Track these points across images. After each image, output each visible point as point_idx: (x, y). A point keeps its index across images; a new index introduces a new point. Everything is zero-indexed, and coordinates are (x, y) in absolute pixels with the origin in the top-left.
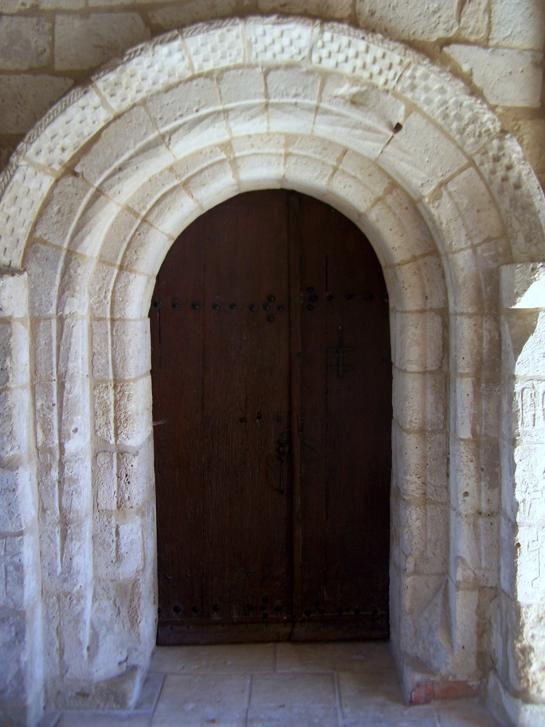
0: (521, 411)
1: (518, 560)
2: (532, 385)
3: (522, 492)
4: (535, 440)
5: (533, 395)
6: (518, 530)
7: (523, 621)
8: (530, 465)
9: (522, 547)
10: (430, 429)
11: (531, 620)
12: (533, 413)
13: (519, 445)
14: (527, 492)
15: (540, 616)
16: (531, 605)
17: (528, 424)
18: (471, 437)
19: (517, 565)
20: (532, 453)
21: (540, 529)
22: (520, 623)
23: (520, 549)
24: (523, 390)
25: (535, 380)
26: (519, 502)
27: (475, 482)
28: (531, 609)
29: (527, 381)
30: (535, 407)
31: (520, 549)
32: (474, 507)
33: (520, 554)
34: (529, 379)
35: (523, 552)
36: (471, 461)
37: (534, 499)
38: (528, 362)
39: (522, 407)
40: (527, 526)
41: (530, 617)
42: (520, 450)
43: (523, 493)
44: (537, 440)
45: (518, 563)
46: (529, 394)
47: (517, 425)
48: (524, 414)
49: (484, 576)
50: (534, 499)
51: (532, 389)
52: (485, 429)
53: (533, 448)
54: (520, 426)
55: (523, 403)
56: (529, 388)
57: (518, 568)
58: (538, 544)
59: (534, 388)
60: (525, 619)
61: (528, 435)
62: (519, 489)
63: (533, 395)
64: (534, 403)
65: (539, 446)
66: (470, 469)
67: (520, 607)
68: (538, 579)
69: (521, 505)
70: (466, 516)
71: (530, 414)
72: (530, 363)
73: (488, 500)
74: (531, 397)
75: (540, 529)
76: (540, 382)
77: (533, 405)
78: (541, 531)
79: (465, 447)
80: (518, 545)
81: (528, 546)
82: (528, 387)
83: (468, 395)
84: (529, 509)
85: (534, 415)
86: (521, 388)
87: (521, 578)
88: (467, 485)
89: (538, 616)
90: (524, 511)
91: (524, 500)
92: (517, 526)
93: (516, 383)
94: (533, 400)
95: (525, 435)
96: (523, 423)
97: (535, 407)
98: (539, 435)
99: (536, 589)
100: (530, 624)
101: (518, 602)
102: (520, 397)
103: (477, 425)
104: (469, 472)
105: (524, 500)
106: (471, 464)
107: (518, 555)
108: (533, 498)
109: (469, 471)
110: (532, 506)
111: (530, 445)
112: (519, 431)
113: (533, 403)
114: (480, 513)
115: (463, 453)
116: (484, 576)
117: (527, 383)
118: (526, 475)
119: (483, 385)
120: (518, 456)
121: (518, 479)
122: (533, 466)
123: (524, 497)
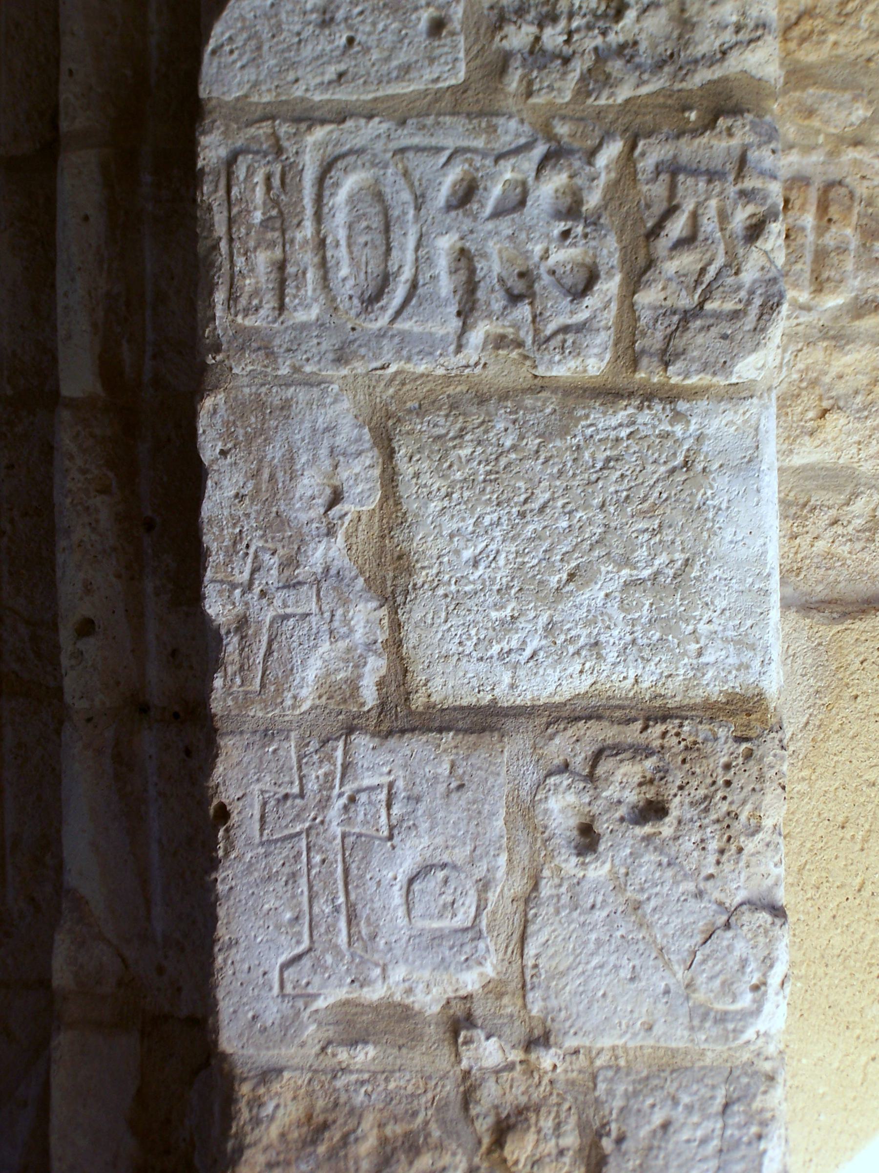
0: (223, 245)
1: (221, 875)
2: (272, 141)
3: (233, 586)
4: (284, 371)
5: (276, 182)
6: (219, 747)
7: (240, 1135)
8: (266, 475)
9: (235, 818)
10: (9, 392)
11: (274, 1131)
12: (278, 253)
13: (216, 387)
14: (257, 590)
15: (319, 1119)
16: (279, 1071)
17: (255, 302)
18: (99, 389)
19: (217, 899)
20: (273, 423)
21: (311, 749)
22: (230, 1145)
23: (227, 831)
24: (231, 161)
25: (285, 120)
26: (223, 631)
27: (119, 576)
28: (276, 1087)
29: (249, 124)
30: (283, 232)
31: (227, 831)
32: (118, 683)
33: (227, 854)
34: (259, 113)
35: (240, 843)
36: (101, 492)
37: (286, 617)
38: (253, 43)
39: (230, 229)
40: (255, 732)
41: (272, 1118)
42: (222, 410)
43: (238, 592)
44: (296, 369)
45: (221, 888)
46: (259, 178)
47: (211, 306)
48: (240, 262)
49: (160, 970)
50: (286, 617)
51: (270, 158)
52: (154, 357)
53: (277, 402)
54: (219, 312)
55: (235, 211)
56: (257, 153)
57: (221, 912)
58: (303, 809)
59: (279, 150)
60: (248, 1128)
61: (254, 345)
62: (220, 576)
63: (276, 182)
64: (281, 213)
65: (302, 395)
66: (97, 521)
67: (234, 1078)
68: (307, 962)
69: (232, 644)
70: (89, 720)
71: (263, 259)
72: (266, 47)
73: (174, 653)
74: (269, 187)
75: (311, 749)
76: (303, 126)
77: (278, 225)
78: (316, 757)
79: (78, 434)
80: (223, 813)
81: (263, 817)
82: (254, 147)
83: (86, 218)
84: (265, 660)
85: (281, 266)
86: (223, 152)
87: (236, 954)
88: (88, 588)
89: (309, 1118)
90: (241, 669)
91: (242, 623)
92: (216, 730)
93: (204, 133)
94: (276, 203)
95: (242, 349)
96: (232, 298)
97: (283, 232)
98: (304, 347)
99: (300, 1004)
100: (265, 1150)
101: (224, 1057)
102: (222, 192)
103: (125, 346)
104: (94, 537)
105: (242, 623)
106: (98, 501)
107: (221, 853)
108: (281, 611)
109: (94, 530)
110: (275, 646)
111: (264, 390)
112: (220, 332)
113: (274, 213)
114: (144, 709)
115: (71, 457)
116: (160, 970)
117: (252, 131)
118: (247, 515)
119: (147, 178)
120: (212, 434)
121: (216, 530)
122: (280, 475)
123: (240, 609)
